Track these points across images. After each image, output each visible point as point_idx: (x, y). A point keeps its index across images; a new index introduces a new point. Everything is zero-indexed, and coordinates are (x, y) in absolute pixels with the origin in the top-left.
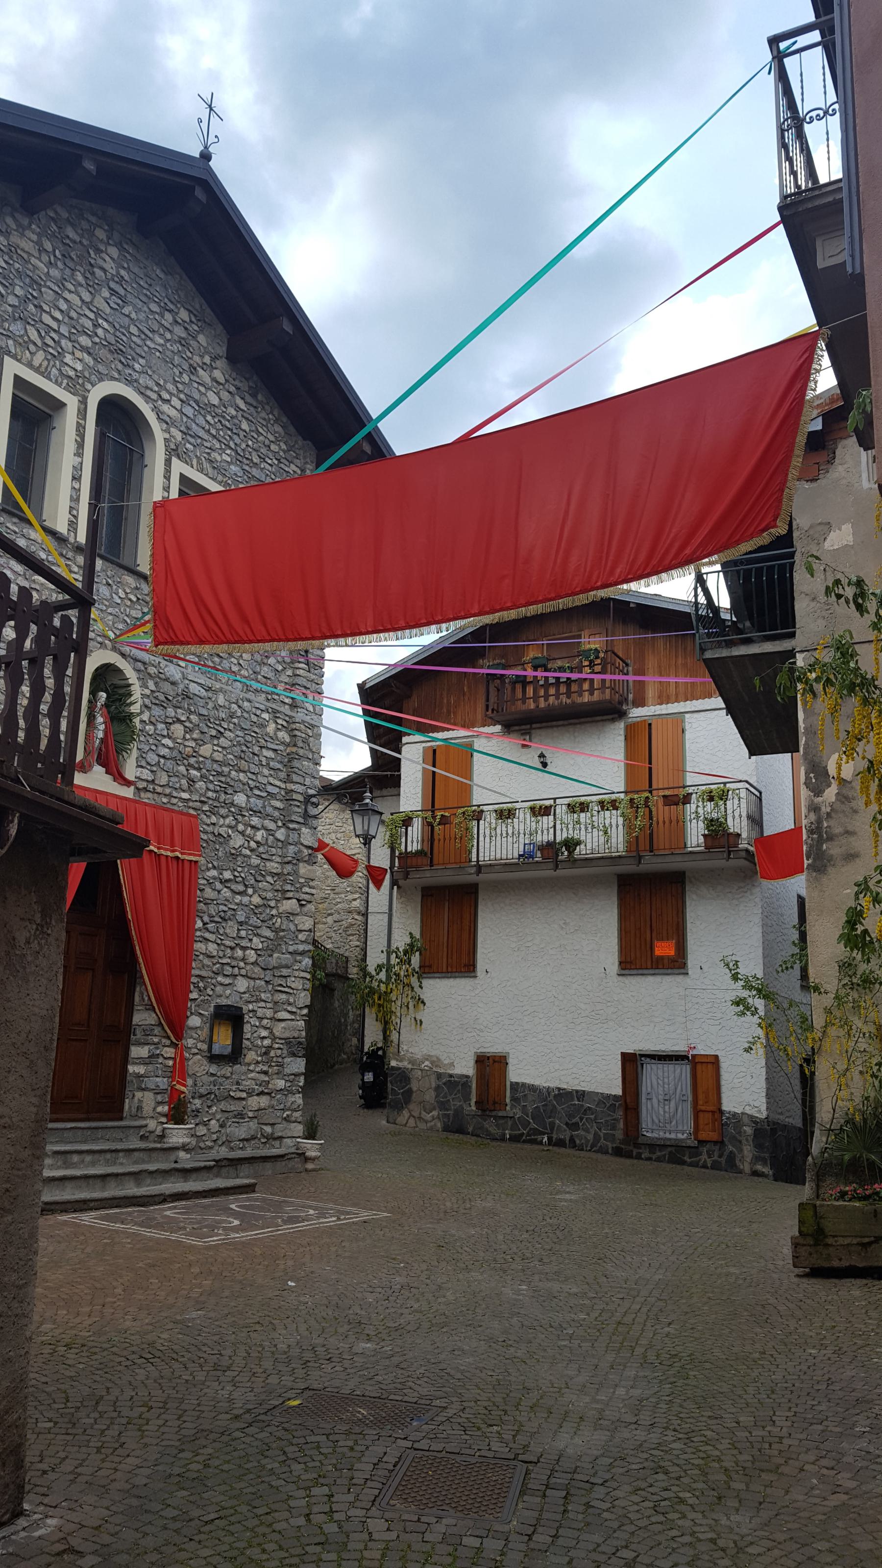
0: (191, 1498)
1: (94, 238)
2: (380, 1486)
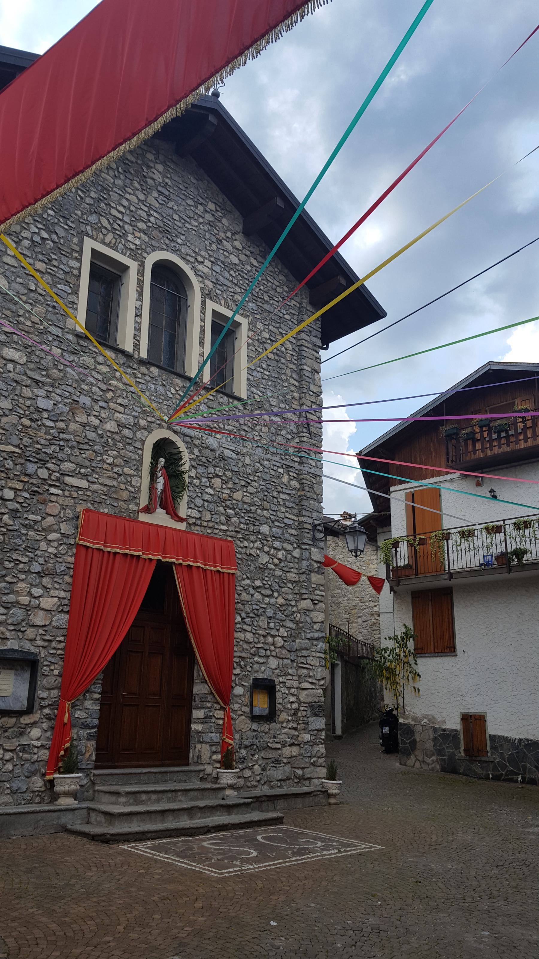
1: (146, 159)
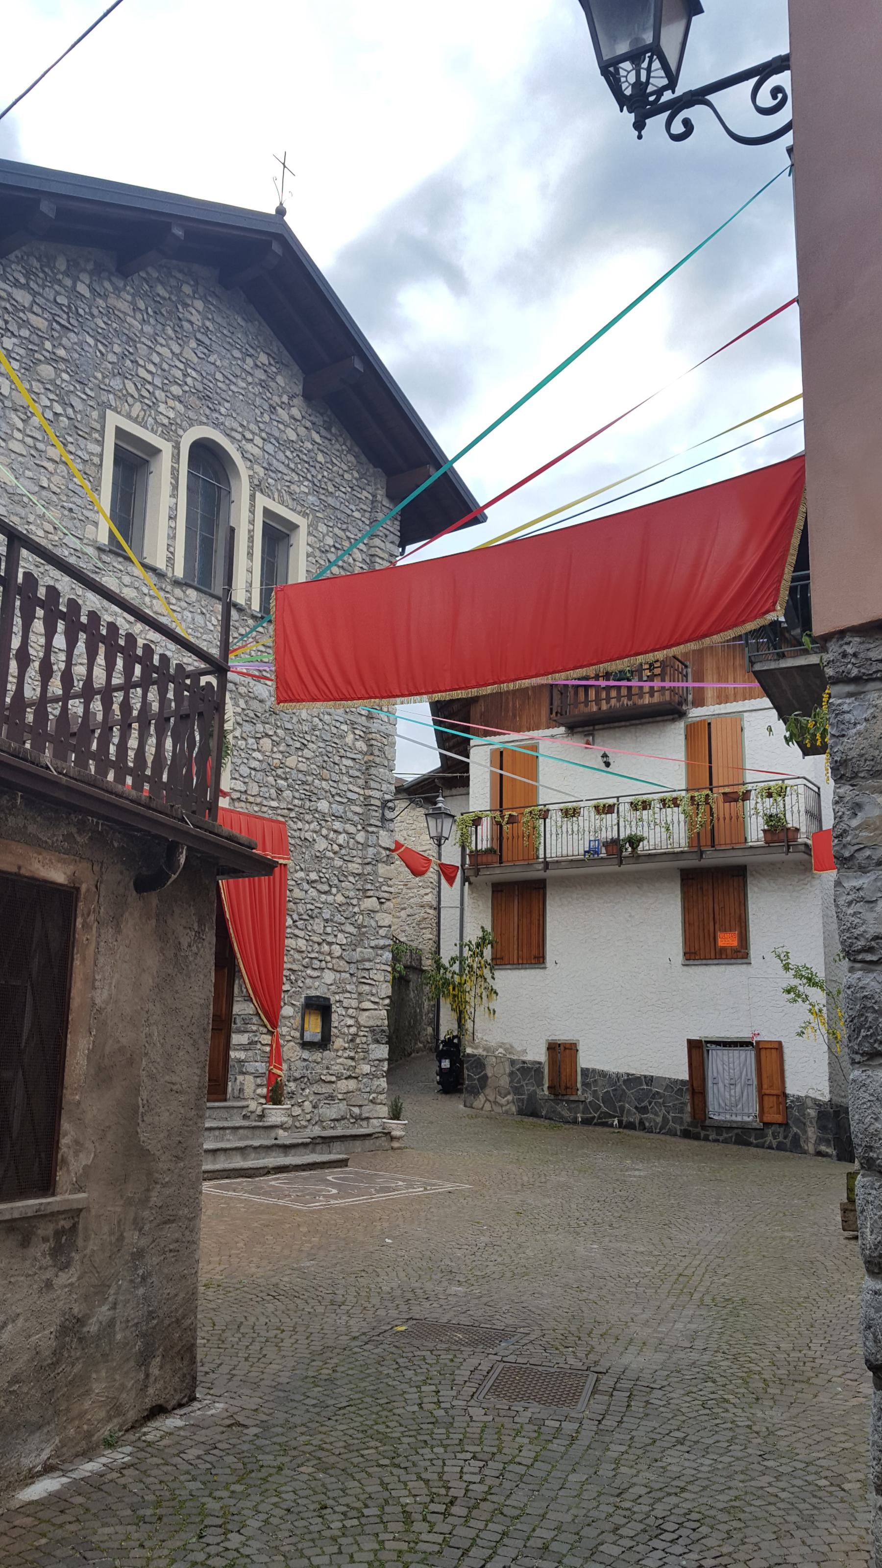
0: (325, 1393)
2: (477, 1386)
